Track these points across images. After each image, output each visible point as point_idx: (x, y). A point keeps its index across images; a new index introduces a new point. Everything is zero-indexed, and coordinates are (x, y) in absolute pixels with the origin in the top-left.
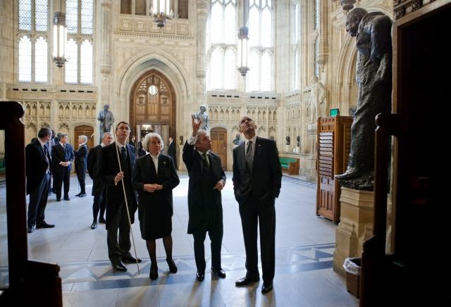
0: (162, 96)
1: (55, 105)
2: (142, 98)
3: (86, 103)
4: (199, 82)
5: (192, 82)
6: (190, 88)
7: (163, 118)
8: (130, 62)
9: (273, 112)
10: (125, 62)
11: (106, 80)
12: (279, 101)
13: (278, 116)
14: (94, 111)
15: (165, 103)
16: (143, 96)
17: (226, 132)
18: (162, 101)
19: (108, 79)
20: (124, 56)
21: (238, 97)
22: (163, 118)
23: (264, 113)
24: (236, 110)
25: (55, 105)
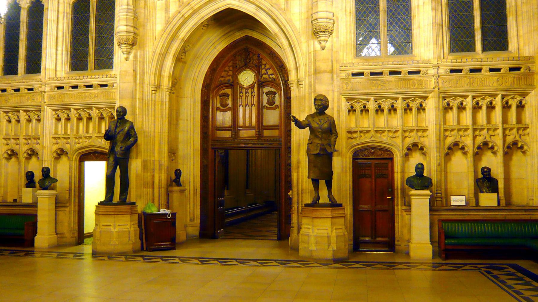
0: (266, 90)
1: (48, 114)
2: (227, 95)
3: (77, 109)
4: (318, 46)
5: (304, 46)
6: (302, 61)
7: (266, 133)
8: (177, 21)
9: (514, 103)
10: (168, 22)
11: (127, 59)
12: (530, 74)
13: (528, 114)
14: (40, 126)
15: (271, 103)
16: (228, 91)
17: (392, 159)
18: (265, 98)
19: (131, 57)
20: (167, 10)
21: (418, 72)
22: (266, 133)
23: (491, 107)
24: (414, 105)
25: (48, 114)
